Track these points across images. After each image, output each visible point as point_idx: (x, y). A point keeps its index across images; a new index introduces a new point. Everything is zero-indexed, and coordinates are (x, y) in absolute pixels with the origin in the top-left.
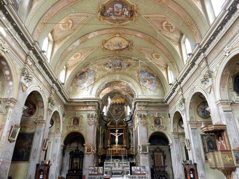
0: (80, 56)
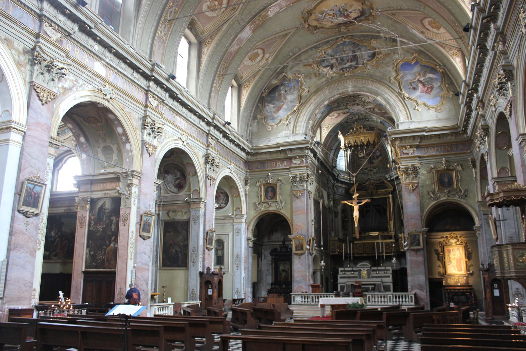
0: (261, 56)
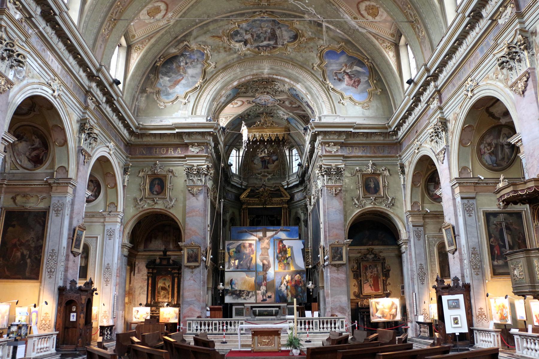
0: (163, 13)
